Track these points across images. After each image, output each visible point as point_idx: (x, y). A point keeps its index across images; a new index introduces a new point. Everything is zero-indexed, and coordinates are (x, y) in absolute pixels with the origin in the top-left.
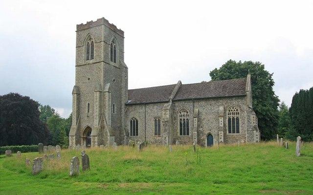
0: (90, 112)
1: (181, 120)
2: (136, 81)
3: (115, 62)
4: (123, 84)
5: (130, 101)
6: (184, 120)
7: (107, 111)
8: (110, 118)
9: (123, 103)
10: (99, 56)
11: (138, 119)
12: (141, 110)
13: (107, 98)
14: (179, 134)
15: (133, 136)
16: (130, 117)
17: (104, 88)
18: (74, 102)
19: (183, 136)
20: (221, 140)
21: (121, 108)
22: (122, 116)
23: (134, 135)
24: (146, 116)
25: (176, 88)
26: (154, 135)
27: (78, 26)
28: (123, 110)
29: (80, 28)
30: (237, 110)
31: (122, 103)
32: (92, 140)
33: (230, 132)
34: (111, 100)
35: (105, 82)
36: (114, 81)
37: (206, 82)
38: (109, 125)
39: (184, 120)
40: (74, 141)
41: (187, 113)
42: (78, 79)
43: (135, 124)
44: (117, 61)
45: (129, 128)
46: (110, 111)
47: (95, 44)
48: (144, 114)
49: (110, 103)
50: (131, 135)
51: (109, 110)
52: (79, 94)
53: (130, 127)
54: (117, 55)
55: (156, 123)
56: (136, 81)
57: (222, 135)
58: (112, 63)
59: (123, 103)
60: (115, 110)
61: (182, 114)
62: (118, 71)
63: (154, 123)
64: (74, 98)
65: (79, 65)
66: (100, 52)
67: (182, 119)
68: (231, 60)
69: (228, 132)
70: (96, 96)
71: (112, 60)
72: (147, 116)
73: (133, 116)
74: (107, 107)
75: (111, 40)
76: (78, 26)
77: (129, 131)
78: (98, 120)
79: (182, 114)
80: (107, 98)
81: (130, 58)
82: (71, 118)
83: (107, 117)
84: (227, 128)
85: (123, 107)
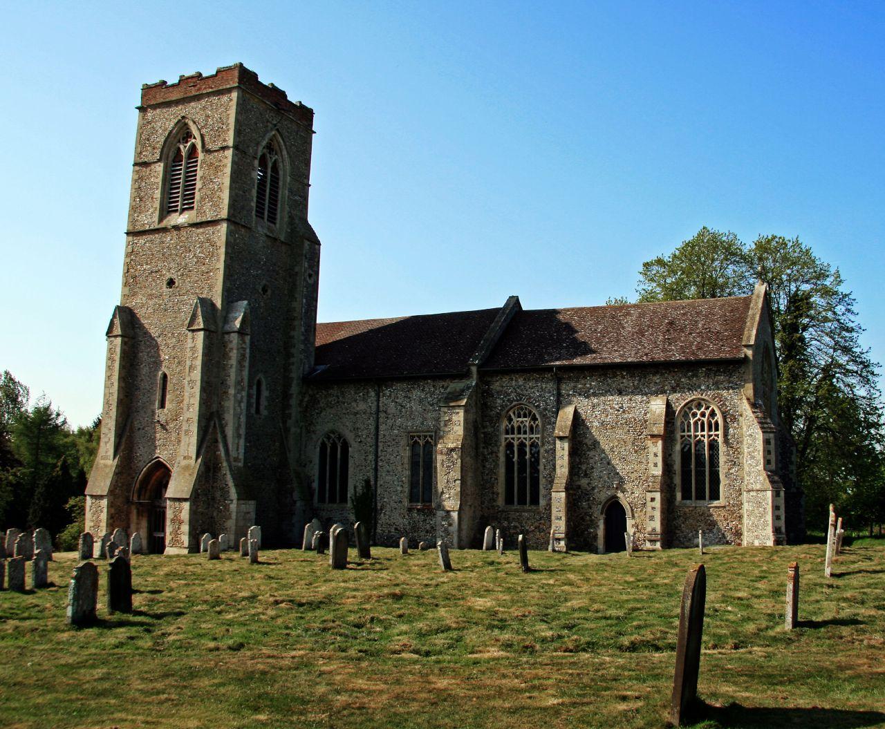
0: (167, 404)
1: (510, 446)
2: (348, 296)
3: (272, 219)
4: (299, 305)
5: (323, 367)
6: (522, 445)
7: (230, 404)
8: (242, 431)
9: (296, 374)
10: (212, 197)
11: (350, 436)
12: (362, 406)
13: (234, 355)
14: (501, 502)
15: (327, 505)
16: (325, 423)
17: (226, 320)
18: (109, 368)
19: (516, 506)
20: (653, 504)
21: (286, 396)
22: (290, 422)
23: (332, 500)
24: (380, 424)
25: (496, 327)
26: (406, 503)
27: (147, 90)
28: (294, 402)
29: (155, 97)
30: (713, 414)
31: (294, 375)
32: (169, 514)
33: (686, 496)
34: (247, 364)
35: (230, 295)
36: (265, 290)
37: (286, 96)
38: (236, 459)
39: (522, 445)
40: (104, 516)
41: (534, 419)
42: (131, 280)
43: (336, 455)
44: (282, 214)
45: (314, 471)
46: (243, 405)
47: (201, 156)
48: (372, 421)
49: (246, 373)
50: (322, 499)
51: (240, 402)
52: (133, 338)
53: (317, 467)
54: (283, 193)
55: (414, 455)
56: (348, 296)
57: (657, 504)
58: (261, 229)
59: (296, 374)
60: (264, 402)
61: (516, 421)
62: (274, 249)
63: (408, 453)
64: (111, 351)
65: (139, 228)
66: (215, 184)
67: (516, 443)
68: (514, 302)
69: (679, 496)
70: (193, 349)
71: (260, 213)
72: (382, 427)
73: (329, 426)
74: (232, 391)
75: (264, 143)
76: (147, 90)
77: (315, 485)
78: (194, 440)
79: (516, 421)
80: (234, 355)
81: (333, 204)
82: (91, 435)
83: (230, 431)
84: (677, 480)
85: (294, 389)
